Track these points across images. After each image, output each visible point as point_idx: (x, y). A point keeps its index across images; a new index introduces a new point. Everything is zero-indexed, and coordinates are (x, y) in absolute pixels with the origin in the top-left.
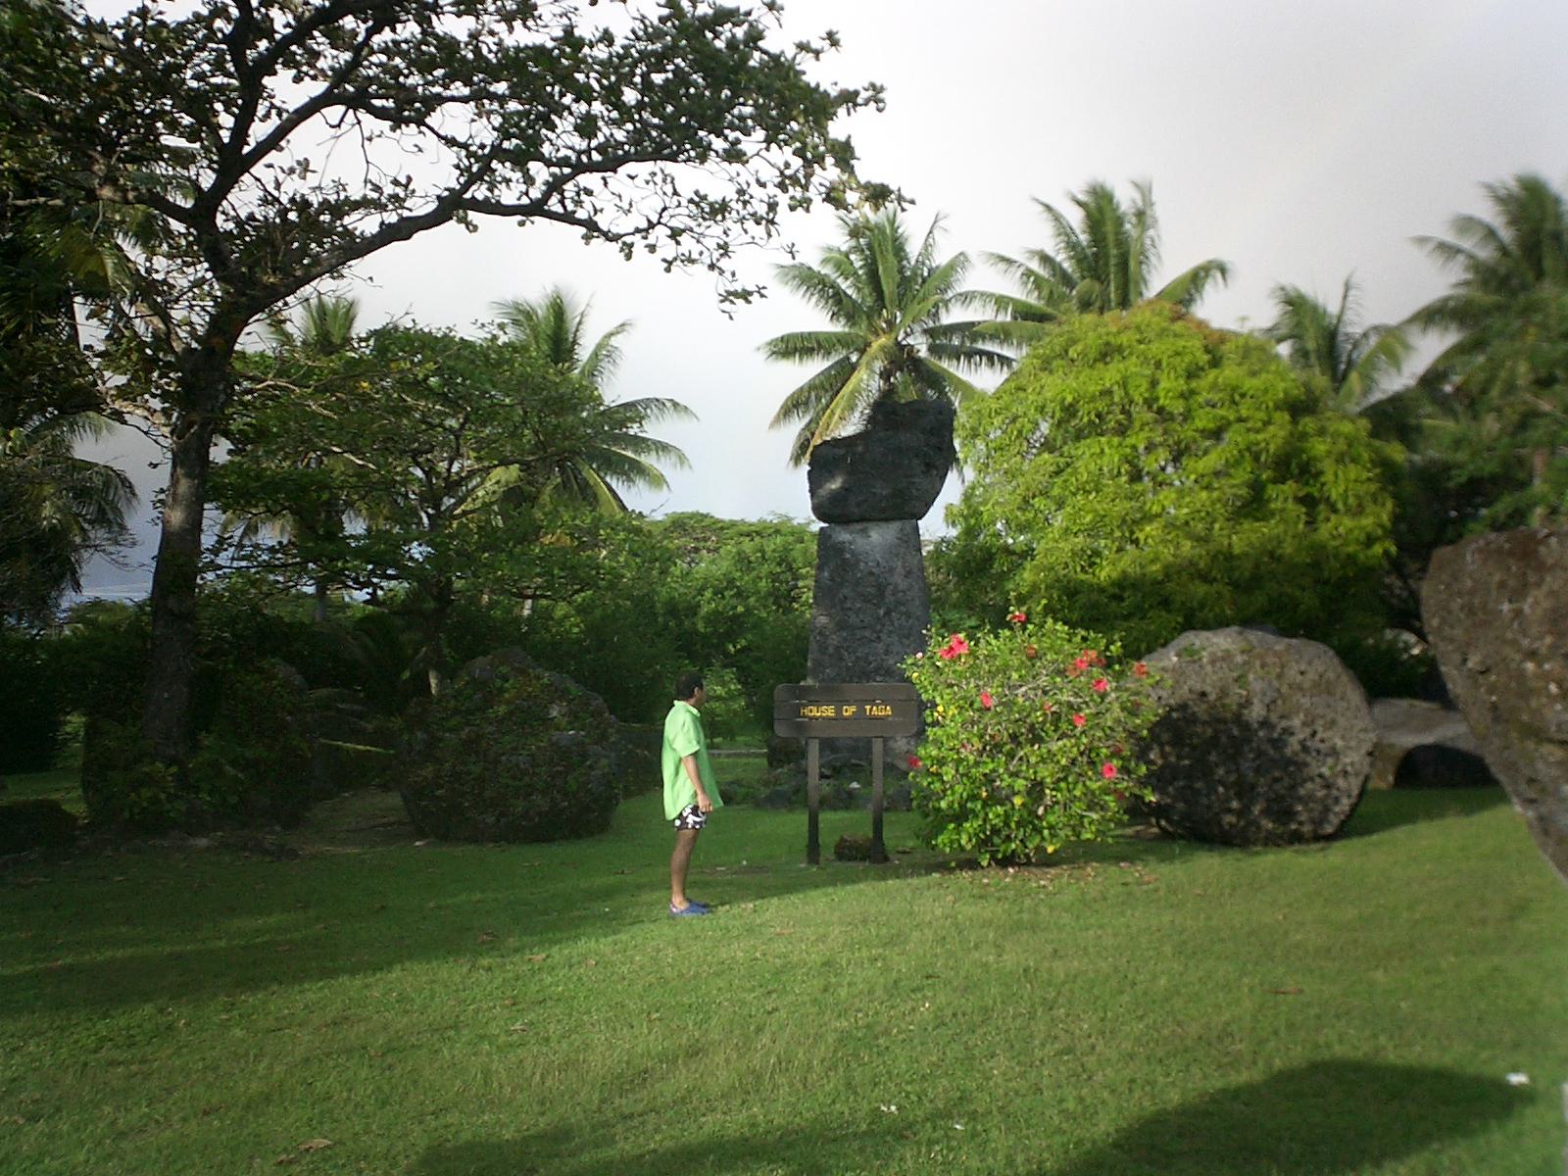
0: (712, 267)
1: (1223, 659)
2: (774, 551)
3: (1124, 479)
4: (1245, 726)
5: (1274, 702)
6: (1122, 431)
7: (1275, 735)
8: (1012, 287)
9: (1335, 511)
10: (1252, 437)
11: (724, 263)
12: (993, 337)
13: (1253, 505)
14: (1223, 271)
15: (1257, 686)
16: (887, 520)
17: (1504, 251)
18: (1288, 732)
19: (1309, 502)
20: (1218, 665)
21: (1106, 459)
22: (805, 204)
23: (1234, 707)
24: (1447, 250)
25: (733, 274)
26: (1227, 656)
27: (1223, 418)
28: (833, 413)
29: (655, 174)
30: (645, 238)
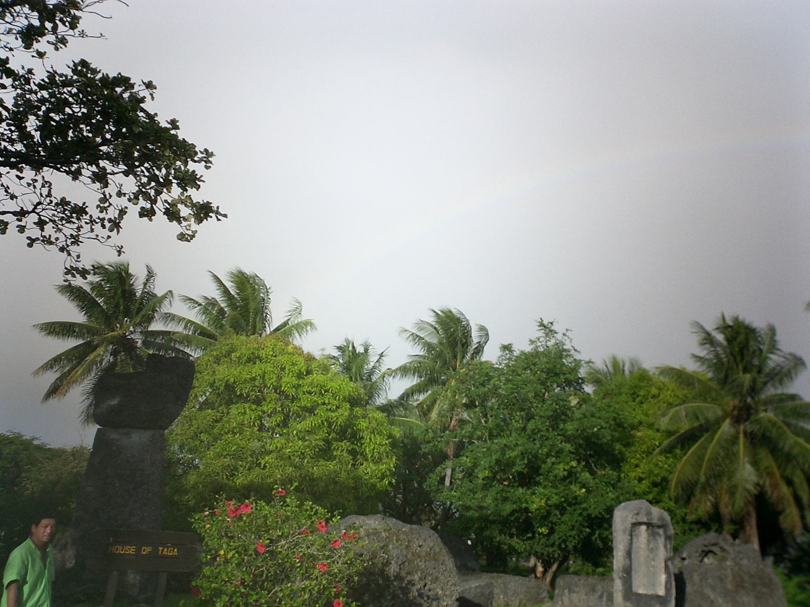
0: (62, 249)
1: (374, 534)
2: (8, 454)
3: (256, 429)
4: (387, 578)
5: (403, 563)
6: (258, 402)
7: (404, 585)
8: (194, 315)
9: (367, 460)
10: (330, 413)
11: (72, 248)
12: (181, 342)
13: (325, 452)
14: (311, 324)
15: (394, 553)
16: (145, 428)
17: (429, 347)
18: (412, 584)
19: (353, 453)
20: (372, 537)
21: (247, 417)
22: (147, 213)
23: (380, 565)
24: (416, 338)
25: (78, 257)
26: (376, 533)
27: (315, 401)
28: (77, 372)
29: (36, 181)
30: (20, 220)
